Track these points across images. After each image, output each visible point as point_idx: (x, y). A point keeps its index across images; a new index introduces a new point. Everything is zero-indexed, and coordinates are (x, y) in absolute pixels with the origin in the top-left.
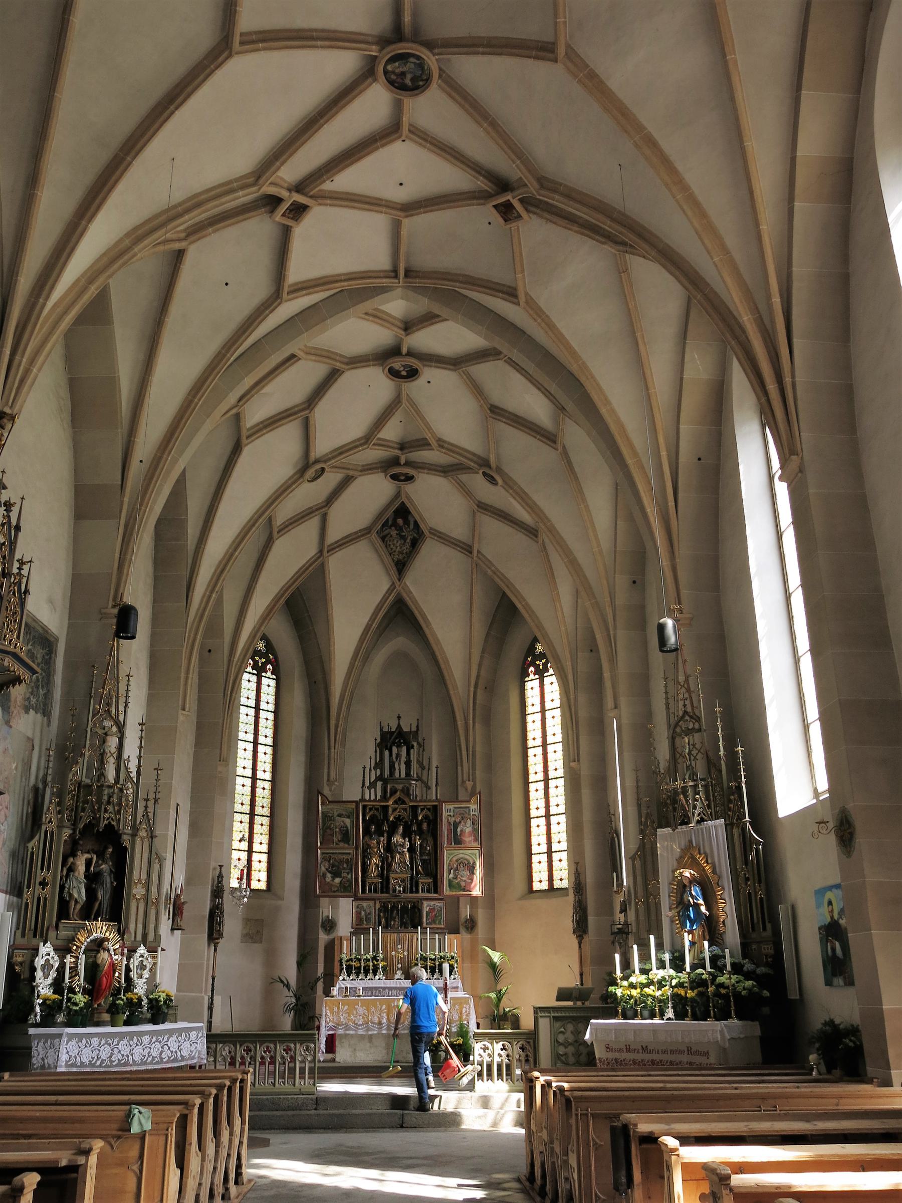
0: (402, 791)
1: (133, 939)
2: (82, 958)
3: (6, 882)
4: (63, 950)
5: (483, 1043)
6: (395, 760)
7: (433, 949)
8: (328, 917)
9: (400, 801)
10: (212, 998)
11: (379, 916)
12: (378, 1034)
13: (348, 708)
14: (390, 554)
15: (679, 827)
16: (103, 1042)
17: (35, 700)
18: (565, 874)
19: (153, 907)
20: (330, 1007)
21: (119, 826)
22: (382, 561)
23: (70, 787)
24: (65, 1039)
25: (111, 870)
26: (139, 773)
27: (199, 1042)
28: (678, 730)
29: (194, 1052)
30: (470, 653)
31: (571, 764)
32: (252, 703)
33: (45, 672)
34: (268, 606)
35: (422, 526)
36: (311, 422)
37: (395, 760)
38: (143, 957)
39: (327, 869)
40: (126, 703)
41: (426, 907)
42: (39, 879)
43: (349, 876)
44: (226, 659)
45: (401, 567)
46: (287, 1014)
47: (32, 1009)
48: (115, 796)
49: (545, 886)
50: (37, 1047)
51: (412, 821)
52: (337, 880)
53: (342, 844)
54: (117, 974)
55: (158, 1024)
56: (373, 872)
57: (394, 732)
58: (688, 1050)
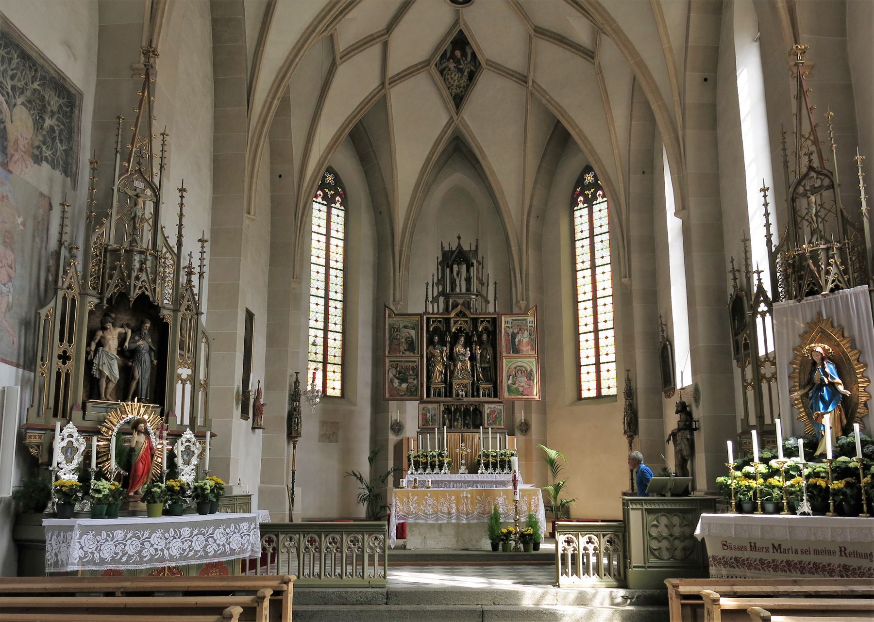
0: (463, 304)
1: (179, 422)
4: (88, 432)
5: (567, 536)
6: (455, 276)
7: (494, 447)
8: (396, 420)
9: (461, 314)
11: (443, 417)
12: (448, 523)
13: (411, 236)
14: (449, 88)
15: (805, 298)
18: (613, 383)
20: (399, 498)
21: (154, 298)
22: (441, 95)
24: (77, 533)
25: (150, 348)
27: (251, 534)
28: (801, 190)
30: (524, 182)
31: (623, 280)
33: (64, 125)
35: (479, 56)
37: (455, 276)
38: (190, 442)
39: (394, 376)
40: (161, 164)
41: (487, 409)
42: (57, 351)
43: (415, 382)
45: (459, 100)
46: (361, 504)
47: (49, 497)
48: (149, 263)
49: (593, 393)
50: (50, 540)
51: (472, 332)
52: (404, 385)
53: (407, 353)
56: (437, 378)
57: (454, 251)
58: (841, 551)
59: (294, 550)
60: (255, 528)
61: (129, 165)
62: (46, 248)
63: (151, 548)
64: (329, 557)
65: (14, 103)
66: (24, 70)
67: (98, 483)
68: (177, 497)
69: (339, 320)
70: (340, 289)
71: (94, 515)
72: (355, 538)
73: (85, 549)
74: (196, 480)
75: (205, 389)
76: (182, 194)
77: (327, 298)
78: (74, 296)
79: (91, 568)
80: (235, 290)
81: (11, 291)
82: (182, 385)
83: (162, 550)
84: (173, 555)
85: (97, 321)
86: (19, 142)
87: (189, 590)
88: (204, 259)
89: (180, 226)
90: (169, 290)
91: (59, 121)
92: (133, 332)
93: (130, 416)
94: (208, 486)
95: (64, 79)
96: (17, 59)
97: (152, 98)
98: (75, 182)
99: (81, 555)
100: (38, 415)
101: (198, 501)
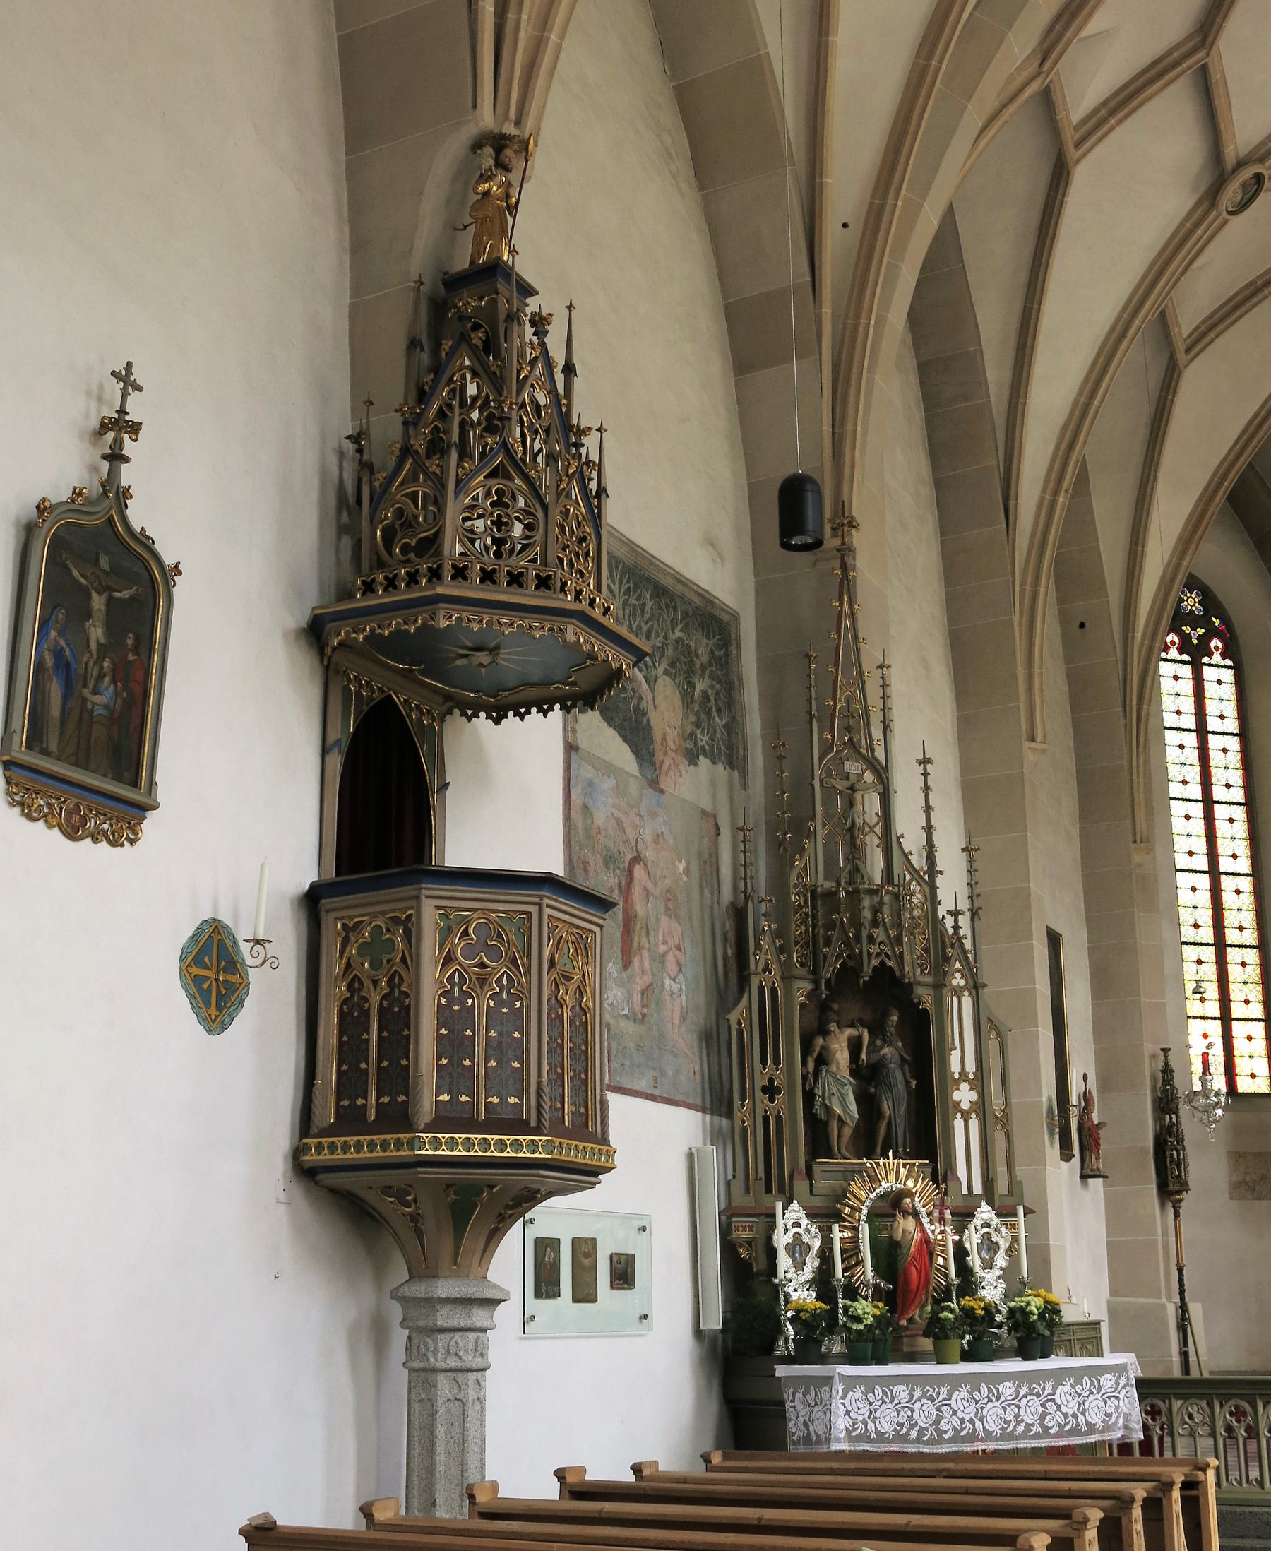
1: (965, 1191)
2: (865, 1229)
3: (699, 1090)
4: (826, 1215)
10: (1183, 1307)
16: (917, 1394)
17: (706, 738)
21: (902, 970)
23: (795, 899)
25: (902, 1059)
27: (1121, 1396)
29: (1114, 1416)
32: (1189, 721)
33: (719, 682)
34: (1191, 515)
36: (1215, 77)
38: (988, 1225)
40: (884, 722)
42: (761, 1082)
44: (1117, 637)
47: (778, 1329)
48: (886, 910)
50: (793, 1401)
54: (940, 1261)
55: (1034, 1359)
62: (718, 903)
67: (854, 1304)
68: (981, 1328)
71: (853, 1360)
74: (1007, 1296)
75: (1004, 1125)
76: (925, 769)
77: (1214, 873)
80: (1022, 899)
83: (972, 1421)
84: (991, 1430)
89: (929, 828)
92: (870, 1032)
93: (884, 1185)
94: (1033, 1308)
100: (747, 1191)
101: (1019, 1335)
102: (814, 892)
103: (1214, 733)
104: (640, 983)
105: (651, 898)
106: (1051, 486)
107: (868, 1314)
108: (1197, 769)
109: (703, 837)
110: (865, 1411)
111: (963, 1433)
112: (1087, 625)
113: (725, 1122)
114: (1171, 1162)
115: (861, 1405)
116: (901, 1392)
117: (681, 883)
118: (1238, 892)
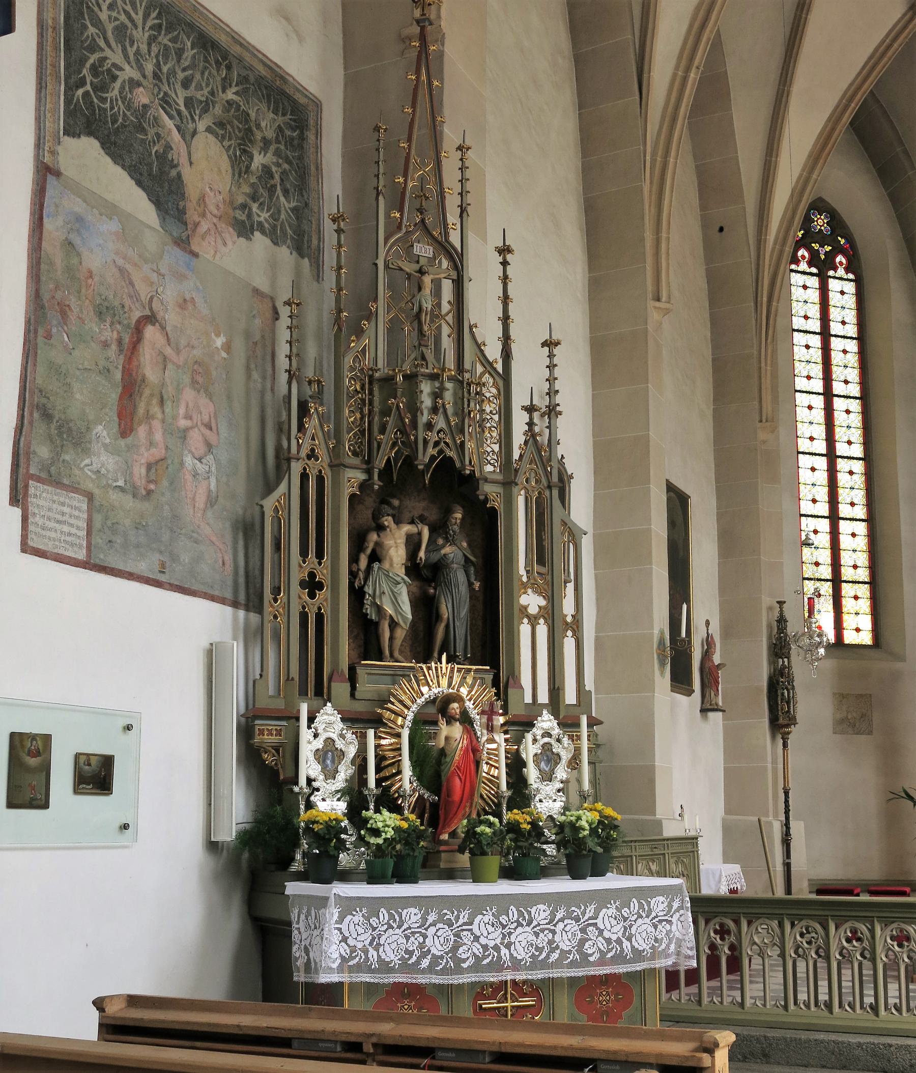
1: (528, 699)
10: (787, 825)
19: (569, 633)
21: (462, 462)
24: (333, 913)
25: (467, 559)
26: (507, 355)
27: (674, 920)
33: (289, 162)
38: (550, 735)
40: (461, 206)
42: (297, 575)
44: (752, 240)
48: (448, 396)
50: (298, 923)
59: (774, 952)
60: (681, 908)
61: (402, 215)
62: (272, 390)
63: (475, 944)
64: (846, 973)
65: (192, 130)
66: (206, 68)
69: (859, 496)
70: (856, 435)
71: (373, 878)
72: (901, 930)
73: (351, 942)
77: (831, 456)
78: (320, 471)
79: (363, 980)
81: (213, 469)
82: (529, 628)
84: (519, 957)
85: (366, 515)
86: (207, 199)
87: (503, 1050)
88: (556, 379)
89: (506, 319)
90: (493, 446)
91: (279, 156)
92: (432, 531)
94: (583, 823)
95: (282, 78)
96: (192, 49)
97: (436, 83)
98: (318, 265)
99: (344, 954)
101: (567, 852)
102: (371, 377)
103: (836, 336)
104: (146, 455)
105: (170, 366)
106: (684, 63)
107: (388, 826)
108: (820, 367)
109: (254, 316)
110: (366, 937)
111: (485, 962)
112: (725, 230)
113: (254, 617)
114: (782, 700)
115: (361, 931)
116: (412, 916)
117: (216, 357)
118: (851, 473)
